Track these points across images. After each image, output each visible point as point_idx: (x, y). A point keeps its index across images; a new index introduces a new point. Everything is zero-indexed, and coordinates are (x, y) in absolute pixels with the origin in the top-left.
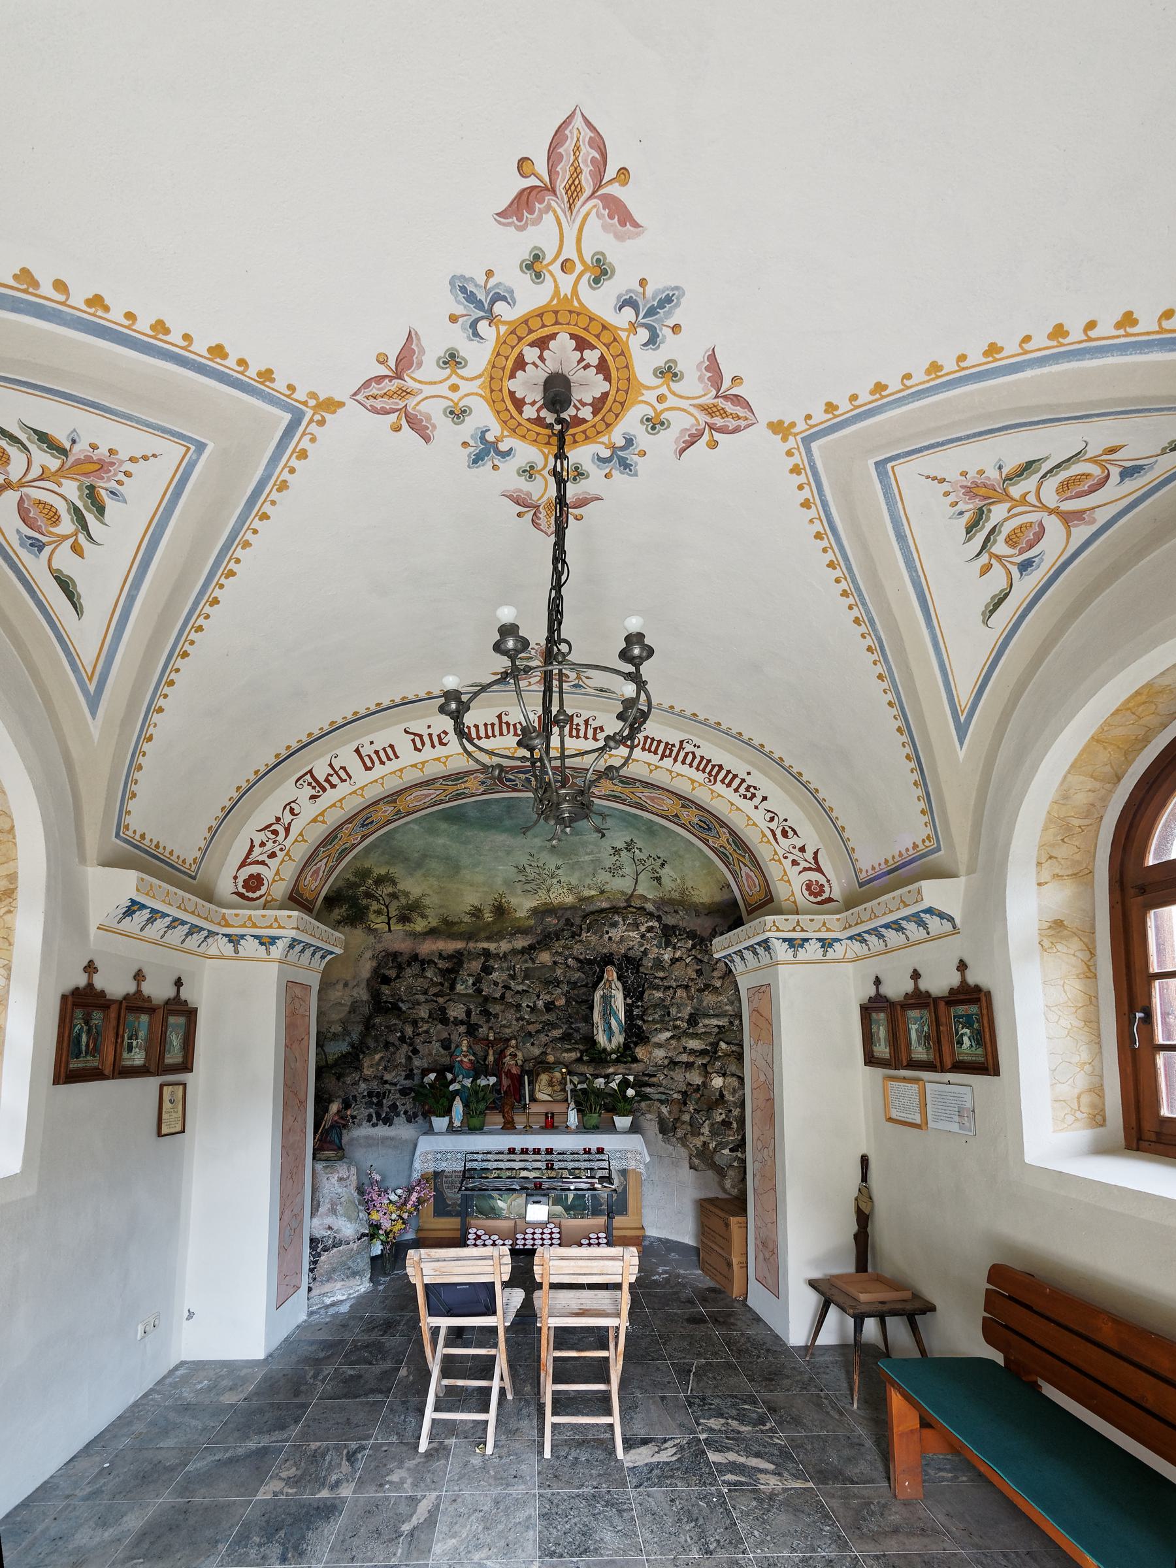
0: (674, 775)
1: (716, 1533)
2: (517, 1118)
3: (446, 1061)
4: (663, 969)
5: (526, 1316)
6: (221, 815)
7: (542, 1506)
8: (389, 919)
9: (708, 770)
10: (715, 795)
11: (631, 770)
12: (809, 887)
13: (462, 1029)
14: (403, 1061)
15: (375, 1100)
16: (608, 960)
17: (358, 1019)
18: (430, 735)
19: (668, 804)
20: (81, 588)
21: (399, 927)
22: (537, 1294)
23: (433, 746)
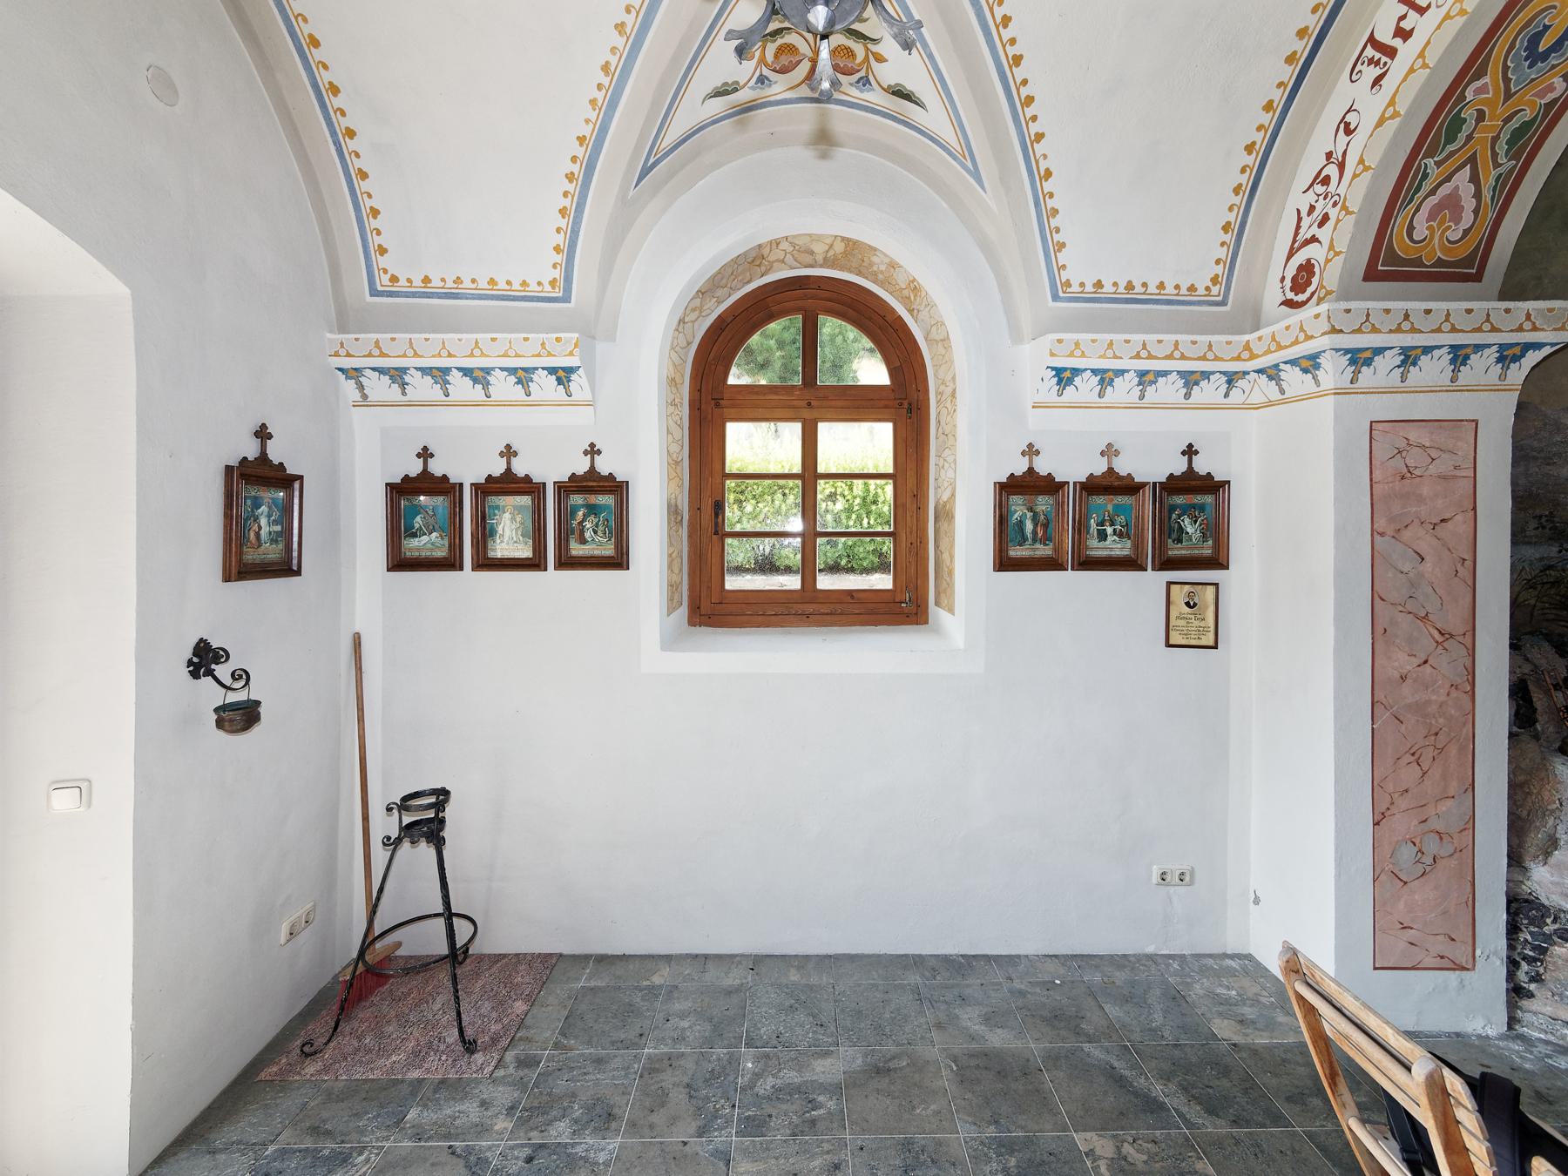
20: (910, 86)
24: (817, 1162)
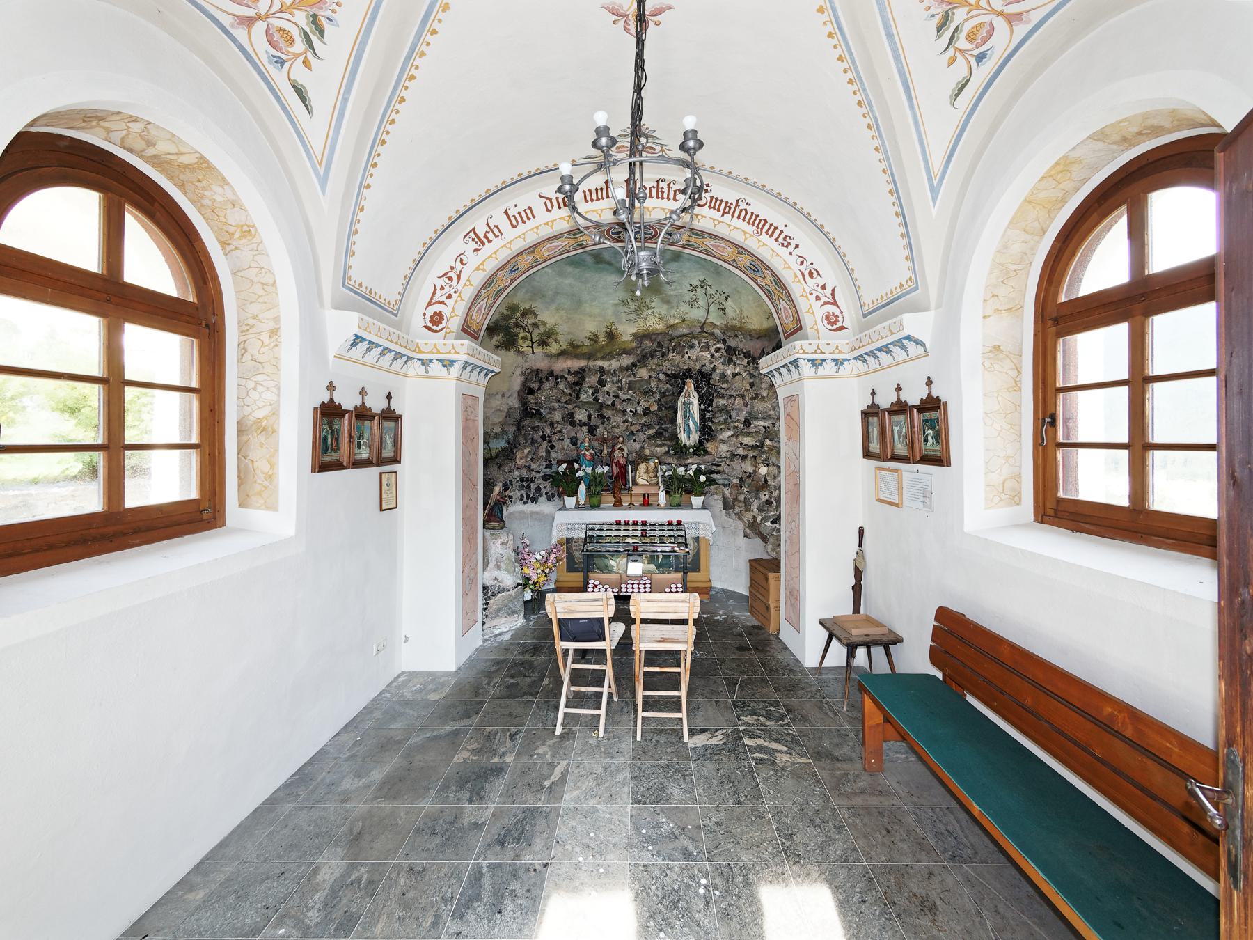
1: (745, 791)
2: (623, 498)
3: (574, 454)
4: (727, 382)
5: (626, 643)
6: (413, 266)
7: (634, 771)
11: (700, 224)
12: (827, 318)
13: (585, 429)
16: (687, 374)
19: (728, 251)
20: (311, 94)
21: (540, 349)
22: (633, 627)
24: (402, 880)
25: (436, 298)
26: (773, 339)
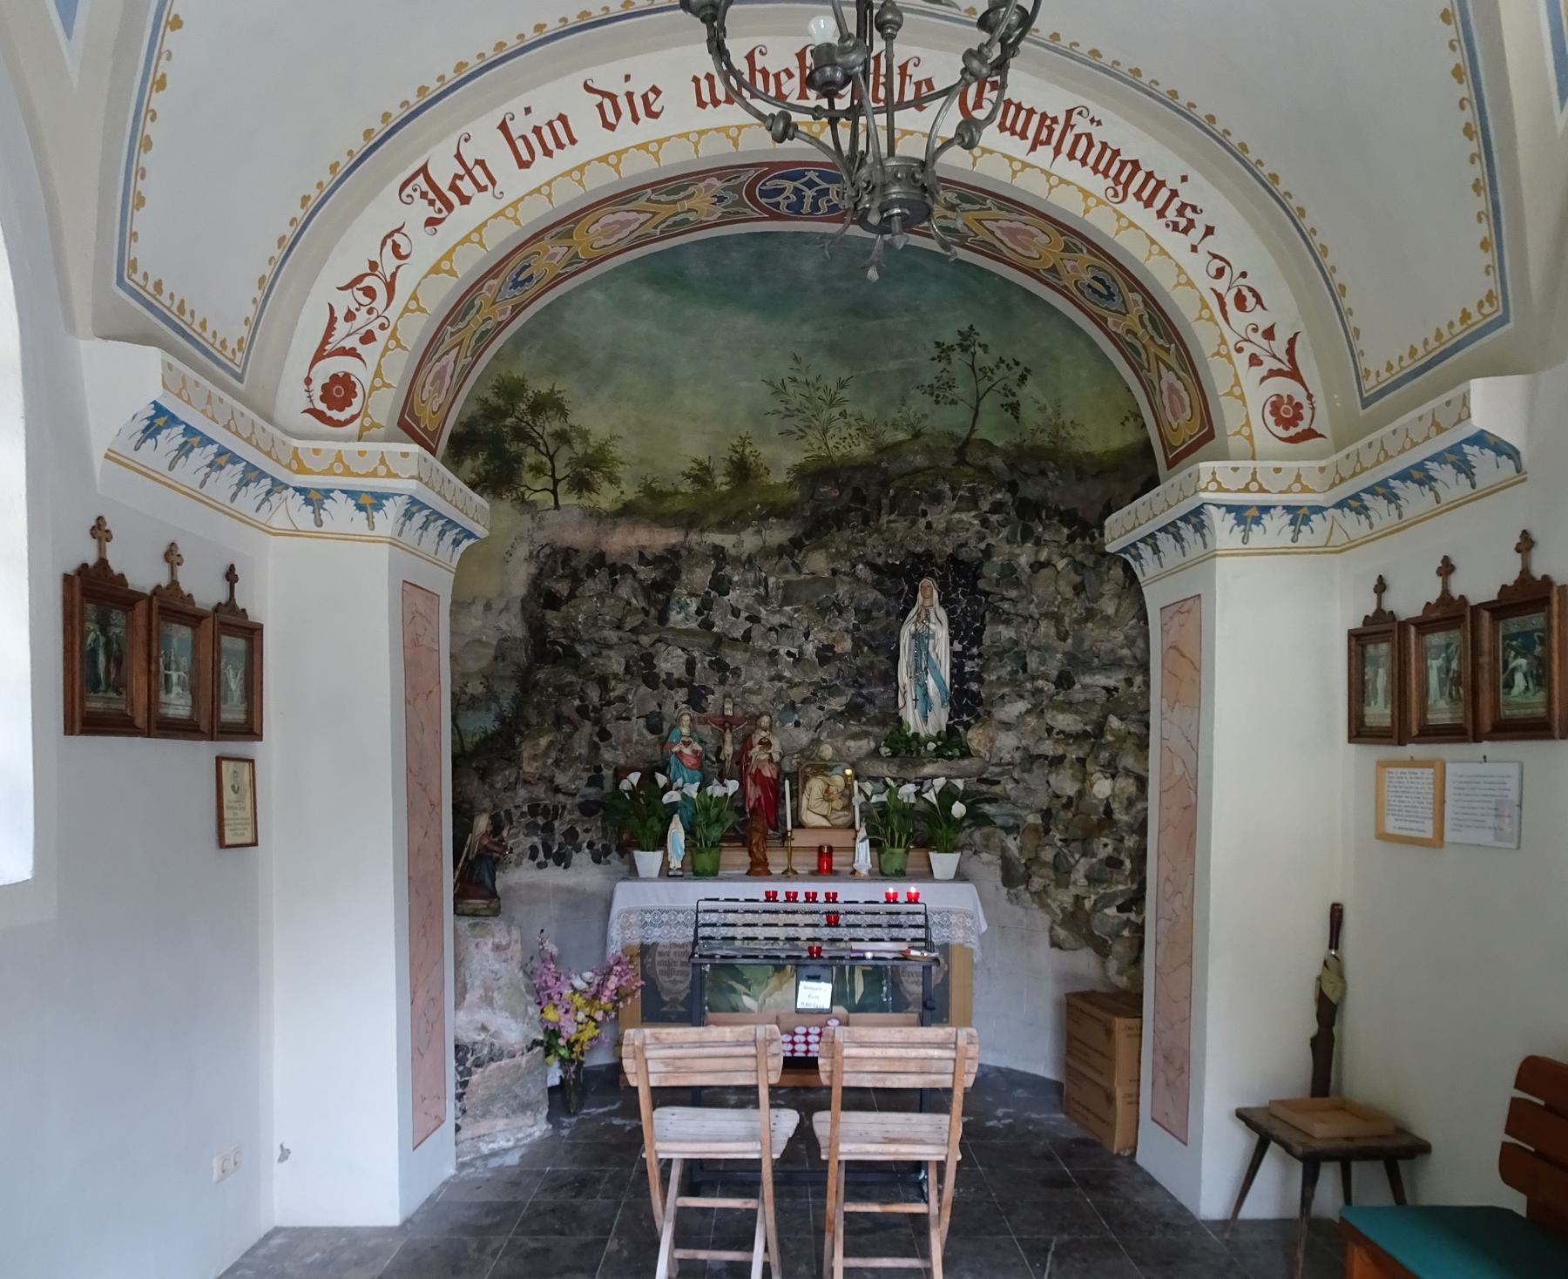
0: (1054, 181)
3: (654, 753)
4: (1017, 584)
6: (278, 254)
8: (556, 482)
9: (1113, 172)
10: (1124, 223)
12: (1275, 409)
13: (681, 694)
14: (584, 751)
15: (541, 821)
17: (508, 672)
18: (630, 95)
19: (1042, 247)
23: (636, 119)
25: (337, 339)
26: (1136, 471)
